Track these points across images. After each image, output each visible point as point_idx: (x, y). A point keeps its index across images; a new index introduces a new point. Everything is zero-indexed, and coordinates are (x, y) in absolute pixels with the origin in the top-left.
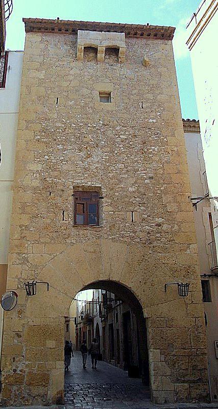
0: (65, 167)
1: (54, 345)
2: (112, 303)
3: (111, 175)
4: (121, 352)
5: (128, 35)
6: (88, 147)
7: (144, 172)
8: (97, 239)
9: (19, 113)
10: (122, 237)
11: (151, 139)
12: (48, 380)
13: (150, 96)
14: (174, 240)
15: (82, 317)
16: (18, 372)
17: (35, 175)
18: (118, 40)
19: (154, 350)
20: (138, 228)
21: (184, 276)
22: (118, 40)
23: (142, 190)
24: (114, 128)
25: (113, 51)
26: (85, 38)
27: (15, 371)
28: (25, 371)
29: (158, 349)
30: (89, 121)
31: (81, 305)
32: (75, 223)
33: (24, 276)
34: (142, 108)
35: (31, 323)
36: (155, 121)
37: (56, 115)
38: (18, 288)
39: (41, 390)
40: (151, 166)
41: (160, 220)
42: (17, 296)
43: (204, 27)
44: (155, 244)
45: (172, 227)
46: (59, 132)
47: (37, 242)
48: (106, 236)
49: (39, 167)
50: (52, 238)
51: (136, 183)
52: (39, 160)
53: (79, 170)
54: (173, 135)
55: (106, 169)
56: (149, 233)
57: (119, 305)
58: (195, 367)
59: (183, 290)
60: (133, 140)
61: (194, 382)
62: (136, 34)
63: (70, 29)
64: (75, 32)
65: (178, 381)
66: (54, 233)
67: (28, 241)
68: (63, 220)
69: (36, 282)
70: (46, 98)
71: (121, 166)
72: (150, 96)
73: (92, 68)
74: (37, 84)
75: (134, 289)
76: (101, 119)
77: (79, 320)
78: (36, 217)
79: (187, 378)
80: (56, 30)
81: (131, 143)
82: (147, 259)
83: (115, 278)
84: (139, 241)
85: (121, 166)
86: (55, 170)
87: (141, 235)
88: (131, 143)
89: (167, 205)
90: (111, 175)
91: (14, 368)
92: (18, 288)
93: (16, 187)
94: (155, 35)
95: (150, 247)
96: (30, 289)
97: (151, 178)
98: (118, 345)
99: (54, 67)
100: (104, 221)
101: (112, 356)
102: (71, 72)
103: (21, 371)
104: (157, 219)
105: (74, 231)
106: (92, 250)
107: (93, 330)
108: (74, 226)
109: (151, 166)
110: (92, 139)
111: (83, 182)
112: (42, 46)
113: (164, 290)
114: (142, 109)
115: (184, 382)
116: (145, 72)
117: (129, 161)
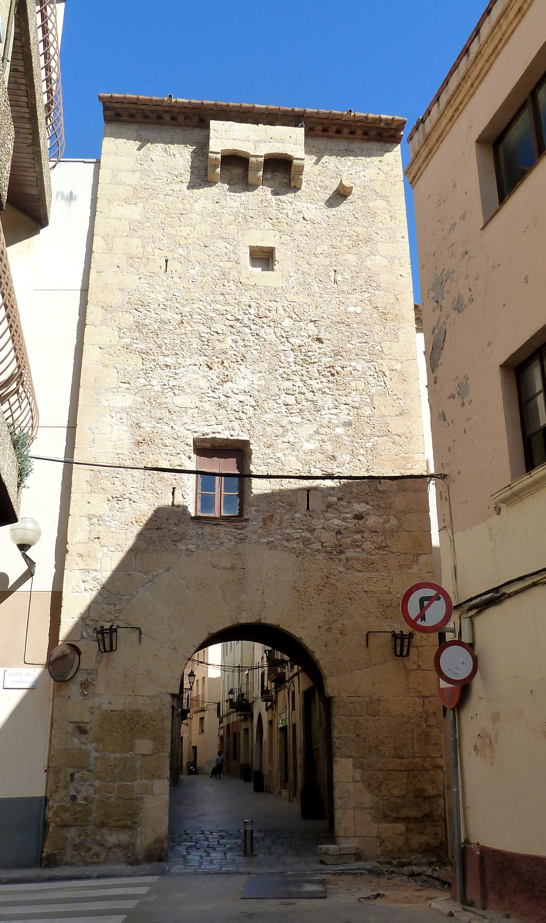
4: (300, 772)
6: (225, 362)
13: (352, 259)
16: (80, 801)
20: (318, 523)
23: (329, 447)
26: (225, 136)
27: (74, 798)
29: (350, 757)
31: (214, 673)
35: (106, 707)
36: (359, 310)
39: (124, 837)
41: (361, 508)
42: (79, 653)
44: (350, 553)
45: (385, 520)
48: (254, 537)
49: (128, 400)
51: (317, 433)
58: (419, 794)
61: (415, 820)
65: (386, 818)
69: (118, 627)
72: (352, 259)
75: (307, 642)
76: (253, 304)
77: (225, 708)
79: (404, 813)
82: (334, 582)
83: (271, 619)
91: (73, 793)
92: (83, 637)
94: (365, 133)
98: (295, 759)
100: (253, 509)
103: (85, 799)
107: (252, 729)
113: (363, 643)
115: (397, 820)
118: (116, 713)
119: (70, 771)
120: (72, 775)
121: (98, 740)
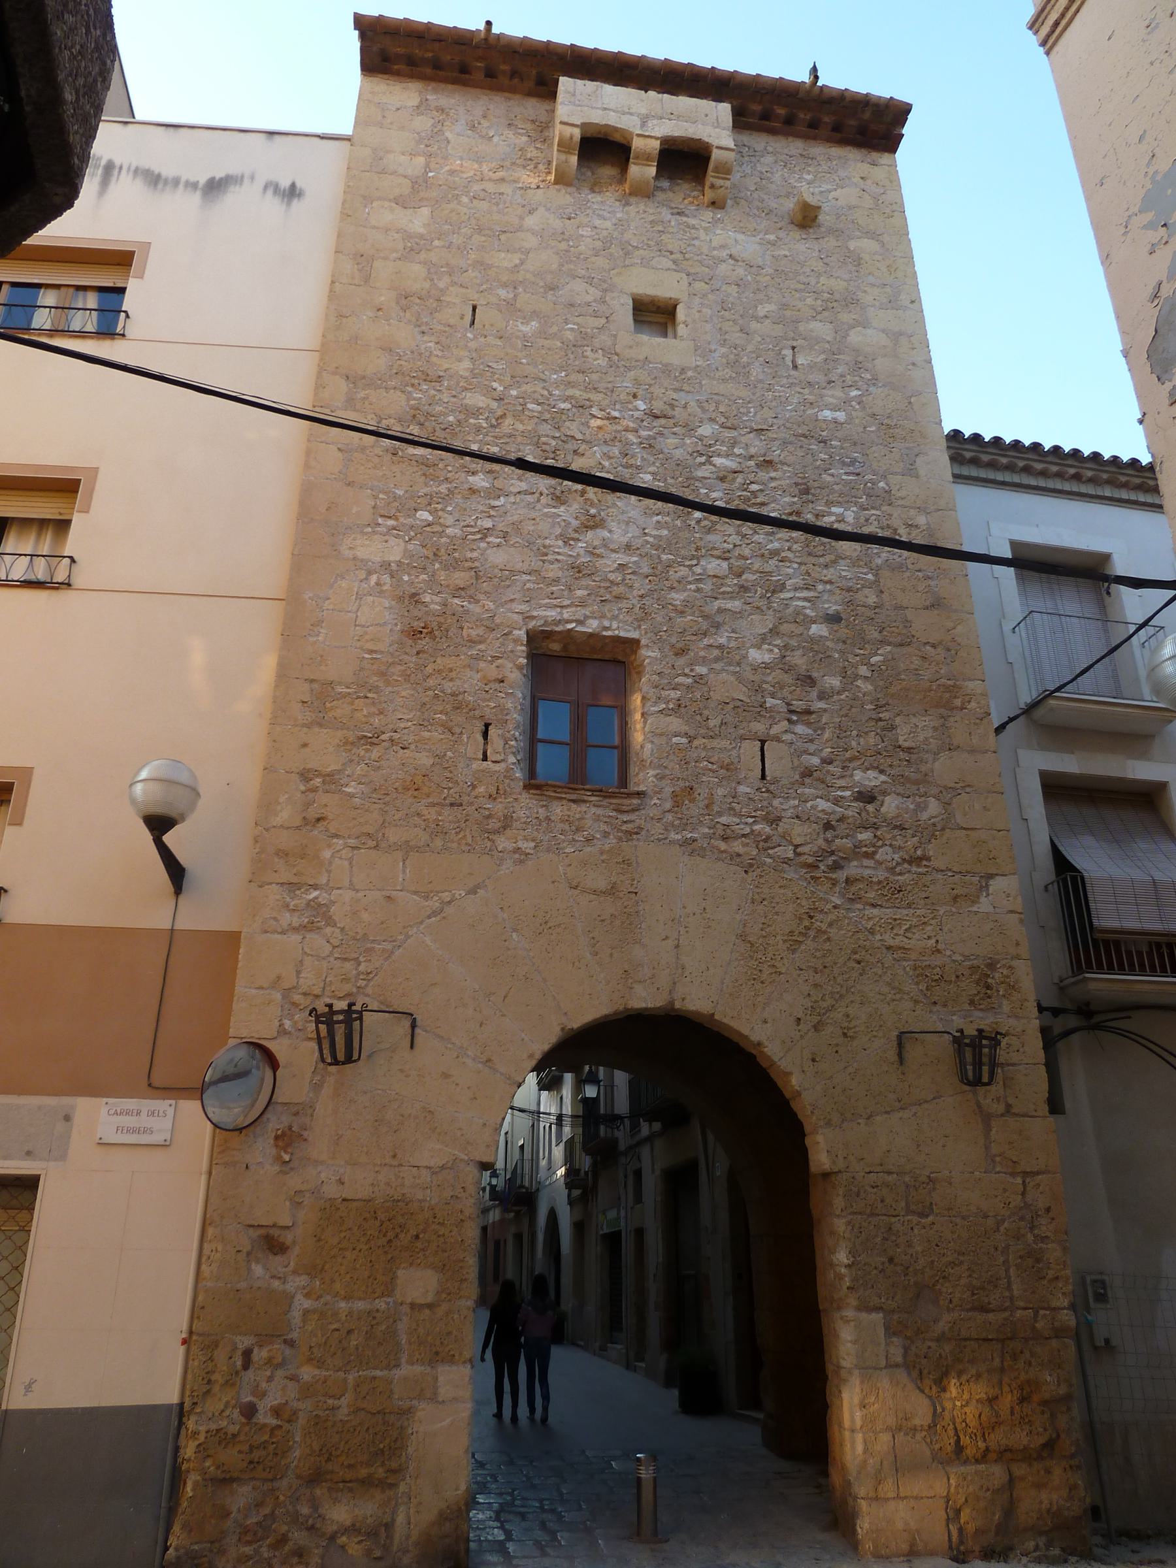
0: (498, 558)
1: (438, 1293)
2: (617, 1134)
3: (677, 597)
5: (741, 121)
7: (805, 594)
8: (620, 839)
9: (325, 350)
10: (725, 839)
11: (829, 479)
12: (397, 1444)
14: (929, 859)
15: (493, 1188)
16: (264, 1417)
17: (374, 578)
18: (709, 122)
19: (864, 1315)
21: (972, 1002)
22: (709, 122)
23: (798, 659)
24: (690, 429)
25: (684, 161)
26: (582, 103)
27: (249, 1411)
28: (295, 1413)
30: (594, 396)
32: (532, 773)
33: (309, 980)
34: (795, 367)
35: (332, 1191)
36: (841, 416)
37: (467, 364)
38: (282, 1032)
40: (830, 574)
41: (870, 779)
43: (1063, 23)
46: (478, 429)
47: (375, 841)
48: (657, 829)
49: (395, 551)
50: (438, 830)
51: (774, 632)
52: (391, 523)
53: (553, 571)
54: (911, 471)
55: (659, 573)
56: (828, 826)
57: (649, 1139)
59: (976, 1059)
60: (763, 475)
62: (766, 116)
63: (523, 70)
64: (547, 91)
66: (447, 811)
67: (336, 836)
68: (485, 758)
70: (431, 303)
71: (714, 566)
72: (821, 329)
73: (605, 212)
74: (396, 251)
78: (371, 740)
80: (479, 76)
81: (754, 487)
82: (824, 927)
84: (791, 855)
85: (714, 566)
86: (456, 565)
87: (799, 832)
88: (754, 487)
89: (898, 720)
90: (677, 597)
93: (297, 617)
94: (837, 128)
95: (834, 883)
96: (340, 1034)
97: (834, 619)
99: (465, 200)
101: (614, 1323)
102: (531, 221)
104: (858, 775)
105: (526, 805)
106: (602, 884)
107: (533, 1235)
108: (527, 787)
109: (830, 574)
110: (606, 464)
111: (566, 616)
112: (423, 123)
113: (892, 1055)
114: (793, 373)
116: (799, 246)
117: (747, 552)
118: (355, 1204)
119: (244, 1342)
120: (247, 1353)
121: (313, 1270)
